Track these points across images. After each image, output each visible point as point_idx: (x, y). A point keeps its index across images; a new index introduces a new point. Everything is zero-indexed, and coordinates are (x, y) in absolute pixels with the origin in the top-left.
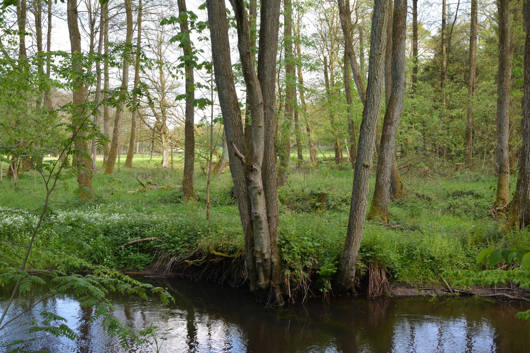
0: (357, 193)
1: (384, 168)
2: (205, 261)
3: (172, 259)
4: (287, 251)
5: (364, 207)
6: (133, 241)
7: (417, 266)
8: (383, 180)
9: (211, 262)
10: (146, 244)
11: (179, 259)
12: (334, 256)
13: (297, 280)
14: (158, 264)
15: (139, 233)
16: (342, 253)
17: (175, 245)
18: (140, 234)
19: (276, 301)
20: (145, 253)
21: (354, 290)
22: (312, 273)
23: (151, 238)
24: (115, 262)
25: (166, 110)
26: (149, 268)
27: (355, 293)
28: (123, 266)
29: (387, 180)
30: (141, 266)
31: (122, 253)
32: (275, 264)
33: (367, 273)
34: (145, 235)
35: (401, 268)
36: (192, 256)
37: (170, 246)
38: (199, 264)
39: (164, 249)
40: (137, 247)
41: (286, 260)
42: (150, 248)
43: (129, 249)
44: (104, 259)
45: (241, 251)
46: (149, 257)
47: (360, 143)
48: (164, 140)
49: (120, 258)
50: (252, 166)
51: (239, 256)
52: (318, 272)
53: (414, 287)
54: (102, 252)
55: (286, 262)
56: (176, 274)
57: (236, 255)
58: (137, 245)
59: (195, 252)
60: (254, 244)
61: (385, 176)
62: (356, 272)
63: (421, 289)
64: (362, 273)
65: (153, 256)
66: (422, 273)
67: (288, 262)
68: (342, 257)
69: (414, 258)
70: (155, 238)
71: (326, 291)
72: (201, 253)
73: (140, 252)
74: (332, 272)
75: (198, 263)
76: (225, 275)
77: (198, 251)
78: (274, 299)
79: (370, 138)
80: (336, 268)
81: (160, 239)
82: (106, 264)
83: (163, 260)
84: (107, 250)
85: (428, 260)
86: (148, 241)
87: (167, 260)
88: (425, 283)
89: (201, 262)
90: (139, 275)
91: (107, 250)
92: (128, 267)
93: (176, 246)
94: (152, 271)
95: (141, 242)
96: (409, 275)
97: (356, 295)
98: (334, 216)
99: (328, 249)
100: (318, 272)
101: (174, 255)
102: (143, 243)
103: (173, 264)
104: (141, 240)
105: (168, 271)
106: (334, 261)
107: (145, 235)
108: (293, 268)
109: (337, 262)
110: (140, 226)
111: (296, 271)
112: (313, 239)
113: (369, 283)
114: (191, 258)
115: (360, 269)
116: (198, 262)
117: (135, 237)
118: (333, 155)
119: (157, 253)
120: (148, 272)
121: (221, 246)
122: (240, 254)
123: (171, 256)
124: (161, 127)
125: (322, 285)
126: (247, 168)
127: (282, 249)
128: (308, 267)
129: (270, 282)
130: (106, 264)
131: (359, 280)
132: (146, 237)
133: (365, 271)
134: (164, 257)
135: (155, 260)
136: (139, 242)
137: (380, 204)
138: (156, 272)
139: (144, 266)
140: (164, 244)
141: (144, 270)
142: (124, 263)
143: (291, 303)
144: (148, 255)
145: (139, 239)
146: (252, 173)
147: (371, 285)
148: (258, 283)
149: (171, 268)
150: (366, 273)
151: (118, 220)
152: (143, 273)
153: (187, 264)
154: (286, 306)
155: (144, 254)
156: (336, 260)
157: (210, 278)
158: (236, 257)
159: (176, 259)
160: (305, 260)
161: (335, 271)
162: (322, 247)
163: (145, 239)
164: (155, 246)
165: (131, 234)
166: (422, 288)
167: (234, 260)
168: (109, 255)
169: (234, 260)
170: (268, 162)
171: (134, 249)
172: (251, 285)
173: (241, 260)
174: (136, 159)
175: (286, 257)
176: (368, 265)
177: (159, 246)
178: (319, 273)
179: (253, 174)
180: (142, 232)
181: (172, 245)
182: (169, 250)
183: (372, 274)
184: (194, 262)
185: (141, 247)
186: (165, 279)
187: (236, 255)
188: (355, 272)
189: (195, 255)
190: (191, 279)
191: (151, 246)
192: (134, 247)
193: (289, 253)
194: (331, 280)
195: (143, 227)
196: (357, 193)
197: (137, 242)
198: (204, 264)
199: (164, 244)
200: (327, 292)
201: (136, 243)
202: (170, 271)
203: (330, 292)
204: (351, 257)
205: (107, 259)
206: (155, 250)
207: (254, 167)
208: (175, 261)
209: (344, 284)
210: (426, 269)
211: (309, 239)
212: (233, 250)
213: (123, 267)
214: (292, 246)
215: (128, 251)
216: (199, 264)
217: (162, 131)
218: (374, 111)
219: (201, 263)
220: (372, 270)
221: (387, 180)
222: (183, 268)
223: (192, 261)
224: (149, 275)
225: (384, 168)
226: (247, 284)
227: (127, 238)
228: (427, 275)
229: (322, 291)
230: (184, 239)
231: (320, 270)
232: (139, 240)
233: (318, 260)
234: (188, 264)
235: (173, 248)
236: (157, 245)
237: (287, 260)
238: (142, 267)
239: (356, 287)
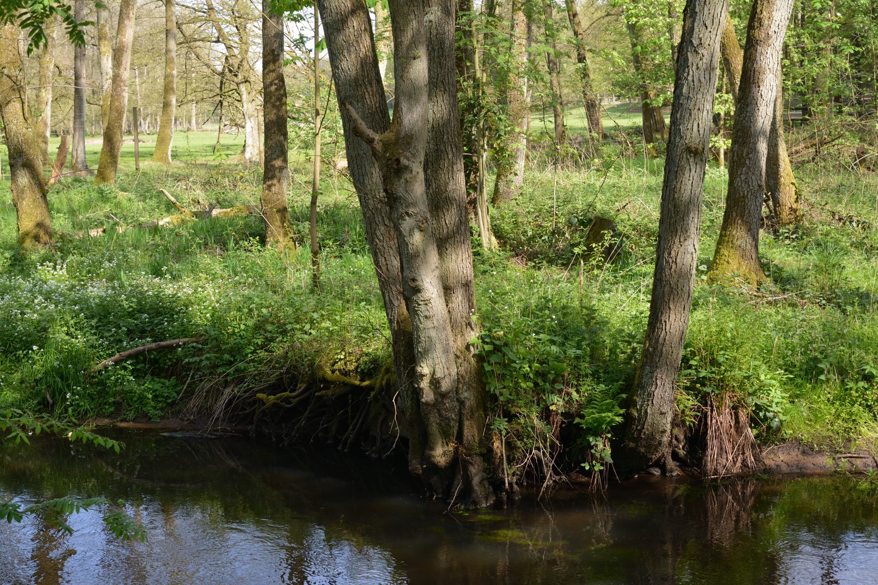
0: (673, 220)
1: (748, 154)
2: (306, 394)
3: (228, 391)
4: (498, 370)
5: (689, 256)
6: (135, 349)
7: (828, 400)
8: (747, 182)
9: (320, 397)
10: (165, 355)
11: (245, 392)
12: (617, 381)
13: (526, 444)
14: (194, 403)
15: (149, 329)
16: (638, 372)
17: (233, 356)
18: (152, 330)
19: (474, 495)
20: (165, 378)
21: (671, 463)
22: (563, 422)
23: (177, 340)
24: (93, 399)
25: (249, 26)
26: (175, 414)
27: (672, 471)
28: (112, 409)
29: (755, 183)
30: (155, 408)
31: (109, 377)
32: (468, 404)
33: (703, 420)
34: (162, 334)
35: (787, 405)
36: (273, 385)
37: (222, 360)
38: (290, 403)
39: (209, 368)
40: (144, 362)
41: (495, 395)
42: (176, 364)
43: (125, 368)
44: (66, 393)
45: (388, 371)
46: (175, 386)
47: (678, 91)
48: (245, 97)
49: (104, 389)
50: (398, 160)
51: (384, 382)
52: (577, 420)
53: (820, 452)
54: (62, 378)
55: (494, 398)
56: (239, 427)
57: (379, 380)
58: (145, 359)
59: (281, 374)
60: (414, 356)
61: (750, 173)
62: (674, 420)
63: (838, 455)
64: (689, 420)
65: (184, 384)
66: (843, 415)
67: (501, 398)
68: (636, 382)
69: (822, 377)
70: (186, 340)
71: (598, 467)
72: (294, 376)
73: (152, 374)
74: (612, 421)
75: (287, 400)
76: (353, 429)
77: (287, 372)
78: (467, 493)
79: (702, 79)
80: (622, 412)
81: (197, 342)
82: (72, 405)
83: (208, 392)
84: (72, 371)
85: (857, 381)
86: (171, 348)
87: (216, 392)
88: (849, 440)
89: (294, 397)
90: (151, 430)
91: (72, 371)
92: (124, 411)
93: (235, 360)
94: (182, 420)
95: (154, 350)
96: (810, 420)
97: (674, 474)
98: (622, 277)
99: (604, 362)
100: (577, 420)
101: (233, 380)
102: (159, 352)
103: (230, 402)
104: (153, 345)
105: (218, 418)
106: (619, 393)
107: (162, 334)
108: (513, 412)
109: (624, 396)
110: (151, 311)
111: (522, 421)
112: (566, 338)
113: (706, 444)
114: (273, 389)
115: (683, 411)
116: (288, 398)
117: (139, 338)
118: (638, 120)
119: (193, 377)
120: (173, 423)
121: (341, 359)
122: (385, 378)
123: (226, 384)
124: (236, 66)
125: (585, 453)
126: (387, 166)
127: (485, 365)
128: (553, 408)
129: (456, 449)
130: (72, 405)
131: (682, 437)
132: (165, 339)
133: (697, 416)
134: (208, 386)
135: (190, 393)
136: (150, 351)
137: (739, 243)
138: (192, 422)
139: (162, 409)
140: (208, 355)
141: (162, 418)
142: (114, 402)
143: (510, 499)
144: (173, 380)
145: (148, 343)
146: (399, 178)
147: (713, 450)
148: (428, 452)
149: (226, 413)
150: (700, 421)
151: (101, 297)
152: (160, 426)
153: (262, 402)
154: (497, 506)
155: (163, 380)
156: (622, 390)
157: (320, 434)
158: (378, 385)
159: (236, 390)
160: (544, 391)
161: (619, 419)
162: (588, 359)
163: (163, 343)
164: (187, 360)
165: (129, 332)
166: (841, 452)
167: (372, 394)
168: (78, 383)
169: (372, 394)
170: (442, 147)
171: (138, 367)
172: (410, 456)
173: (388, 389)
174: (177, 140)
175: (495, 386)
176: (704, 399)
177: (197, 359)
178: (579, 424)
179: (402, 180)
180: (157, 325)
181: (227, 356)
182: (220, 370)
183: (714, 421)
184: (278, 399)
185: (156, 361)
186: (211, 439)
187: (378, 381)
188: (669, 419)
189: (280, 379)
190: (274, 439)
191: (179, 360)
192: (138, 363)
193: (502, 377)
194: (610, 440)
195: (159, 314)
196: (673, 220)
197: (144, 351)
198: (304, 403)
199: (208, 355)
200: (601, 471)
201: (141, 353)
202: (224, 420)
203: (608, 474)
204: (659, 383)
205: (73, 394)
206: (189, 370)
207: (404, 161)
208: (234, 397)
209: (643, 450)
210: (853, 405)
211: (555, 339)
212: (369, 369)
213: (112, 413)
214: (509, 359)
215: (122, 372)
216: (290, 403)
217: (240, 77)
218: (712, 7)
219: (294, 401)
220: (715, 413)
221: (755, 183)
222: (255, 410)
223: (272, 397)
224: (175, 431)
225: (748, 154)
226: (401, 455)
227: (121, 341)
228: (854, 421)
229: (587, 468)
230: (256, 341)
231: (582, 417)
232: (148, 346)
233: (578, 392)
234: (264, 404)
235: (230, 363)
236: (193, 356)
237: (497, 392)
238: (159, 413)
239: (675, 456)
